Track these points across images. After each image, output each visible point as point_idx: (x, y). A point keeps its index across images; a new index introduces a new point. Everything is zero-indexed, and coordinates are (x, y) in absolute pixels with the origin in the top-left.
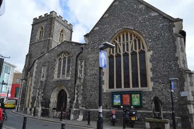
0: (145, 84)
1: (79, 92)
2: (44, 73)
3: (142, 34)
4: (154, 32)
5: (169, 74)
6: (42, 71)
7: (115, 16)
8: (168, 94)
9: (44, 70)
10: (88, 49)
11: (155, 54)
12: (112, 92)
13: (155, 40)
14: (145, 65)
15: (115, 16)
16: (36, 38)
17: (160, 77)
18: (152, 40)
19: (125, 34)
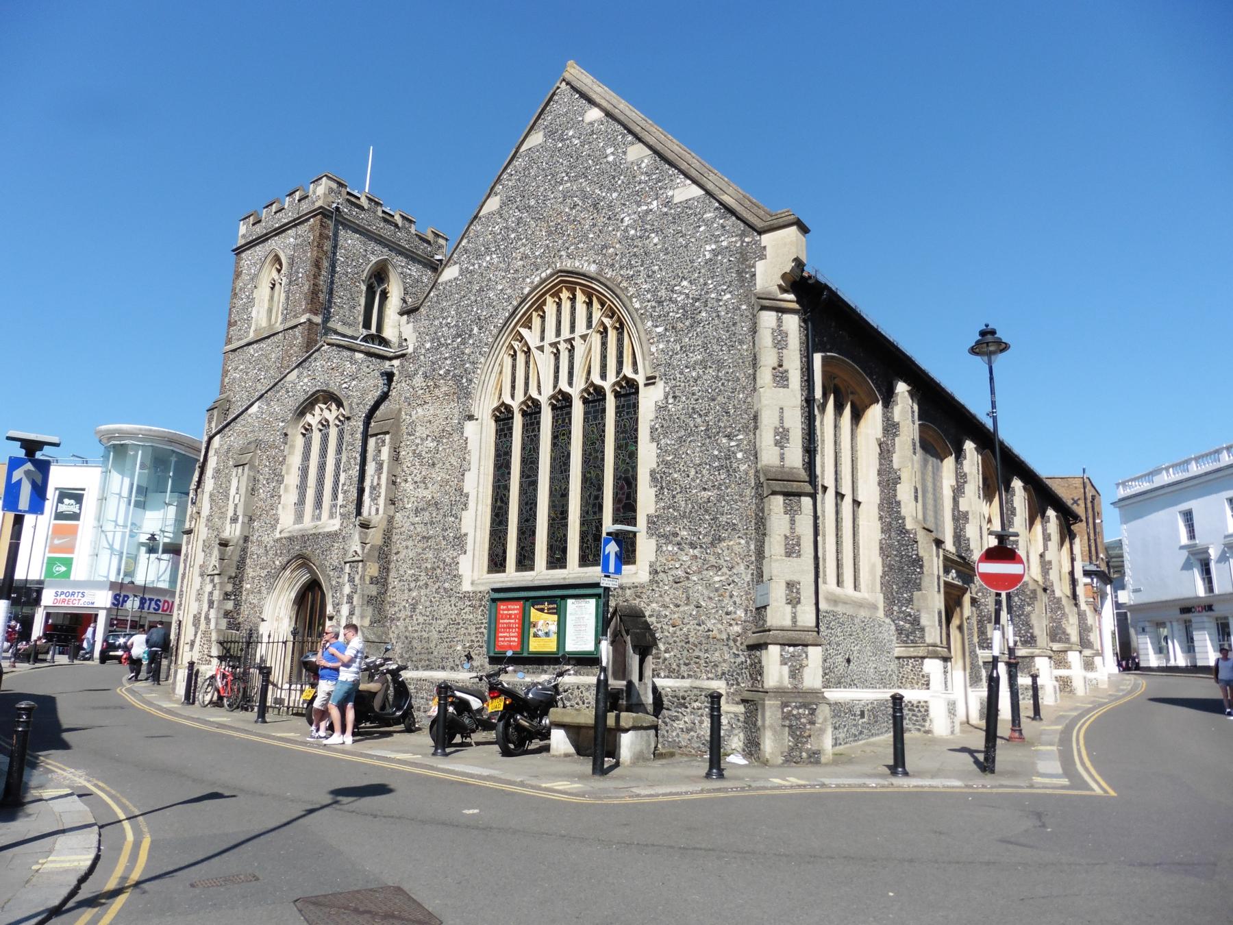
0: (627, 553)
1: (356, 592)
2: (237, 501)
3: (630, 298)
4: (679, 285)
5: (720, 498)
6: (233, 491)
7: (528, 208)
8: (710, 598)
9: (238, 489)
10: (410, 377)
11: (675, 397)
12: (495, 590)
13: (679, 325)
14: (633, 455)
15: (528, 208)
16: (249, 319)
17: (684, 517)
18: (666, 329)
19: (565, 295)
